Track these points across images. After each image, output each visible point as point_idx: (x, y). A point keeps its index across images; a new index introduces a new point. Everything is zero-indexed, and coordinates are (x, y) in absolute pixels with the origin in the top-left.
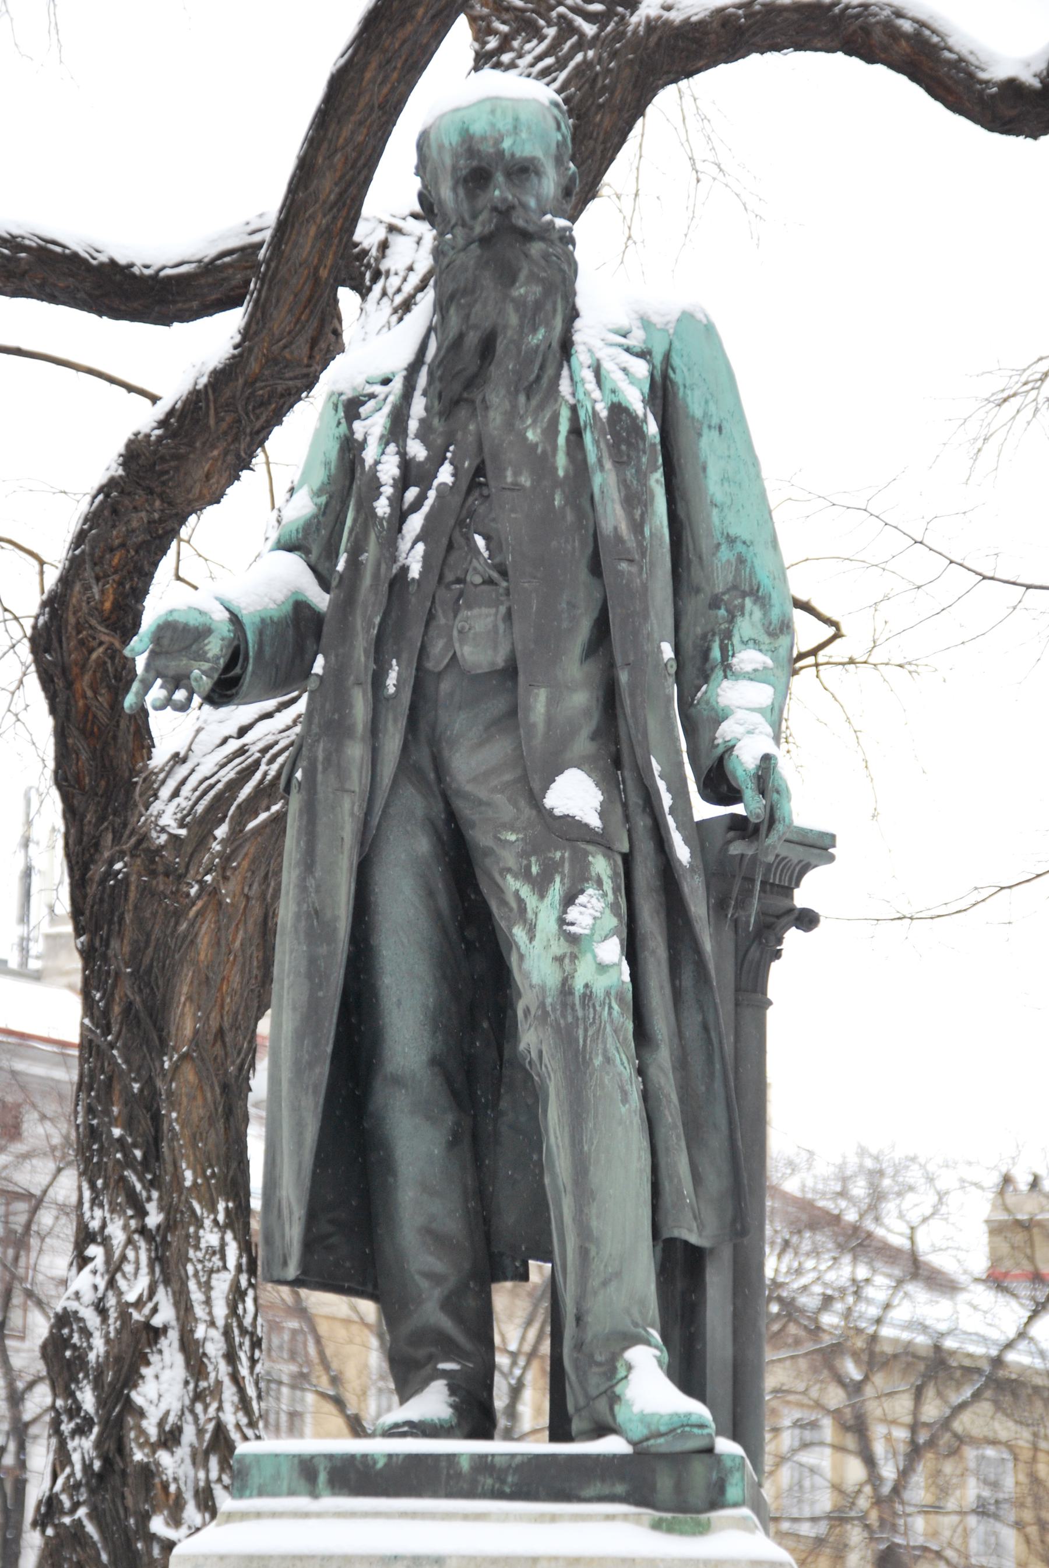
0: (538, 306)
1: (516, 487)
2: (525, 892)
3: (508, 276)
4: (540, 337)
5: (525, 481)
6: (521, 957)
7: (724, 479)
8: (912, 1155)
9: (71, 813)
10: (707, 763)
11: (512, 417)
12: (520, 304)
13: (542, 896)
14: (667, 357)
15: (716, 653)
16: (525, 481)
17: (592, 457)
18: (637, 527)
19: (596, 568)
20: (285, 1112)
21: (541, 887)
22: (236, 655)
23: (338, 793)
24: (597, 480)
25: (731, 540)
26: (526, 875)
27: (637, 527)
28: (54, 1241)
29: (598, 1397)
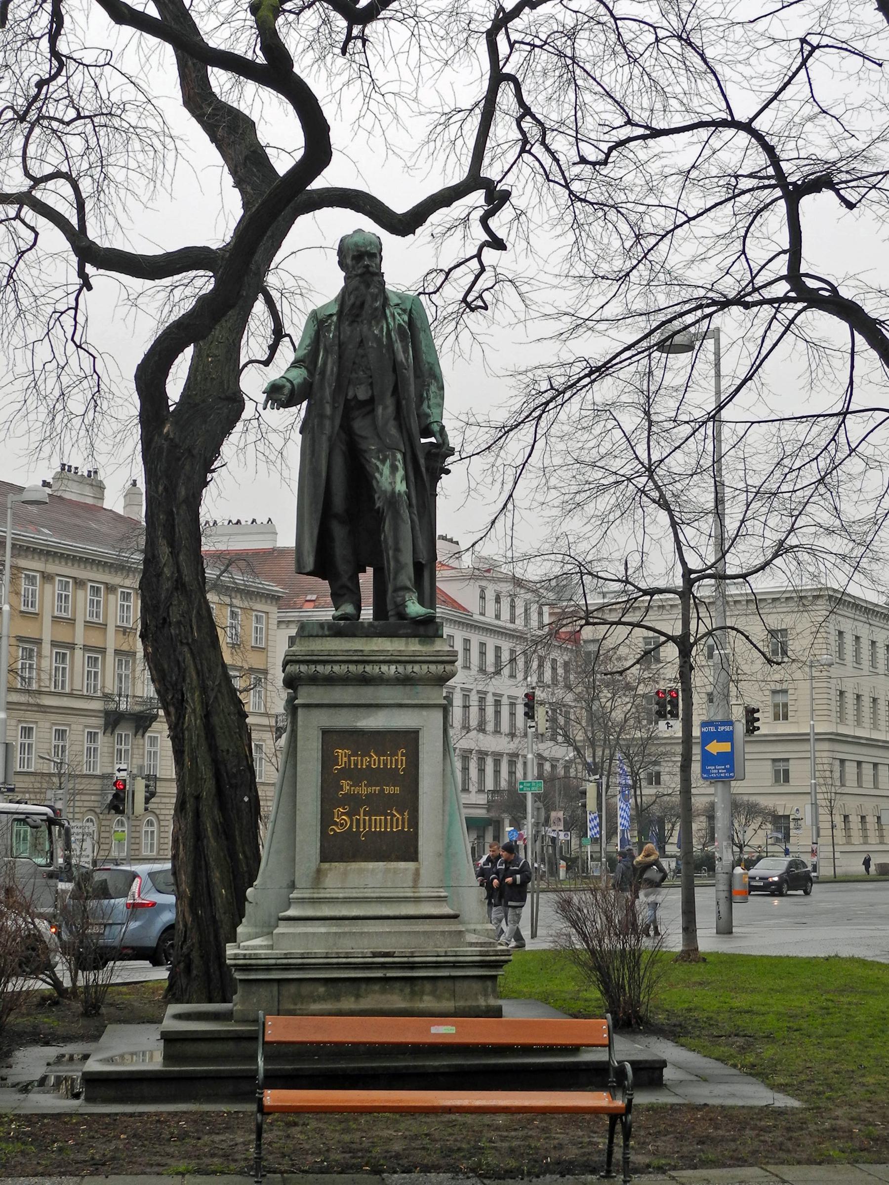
0: (377, 295)
1: (372, 347)
2: (378, 463)
3: (368, 286)
4: (218, 875)
5: (375, 345)
6: (378, 482)
7: (426, 346)
8: (262, 519)
9: (811, 962)
10: (423, 426)
11: (370, 328)
12: (372, 295)
13: (384, 465)
14: (411, 310)
15: (425, 395)
16: (375, 345)
17: (394, 339)
18: (407, 359)
19: (394, 370)
20: (212, 843)
21: (383, 462)
22: (292, 391)
23: (265, 1111)
24: (396, 346)
25: (429, 363)
26: (378, 459)
27: (407, 359)
28: (663, 224)
29: (672, 857)
